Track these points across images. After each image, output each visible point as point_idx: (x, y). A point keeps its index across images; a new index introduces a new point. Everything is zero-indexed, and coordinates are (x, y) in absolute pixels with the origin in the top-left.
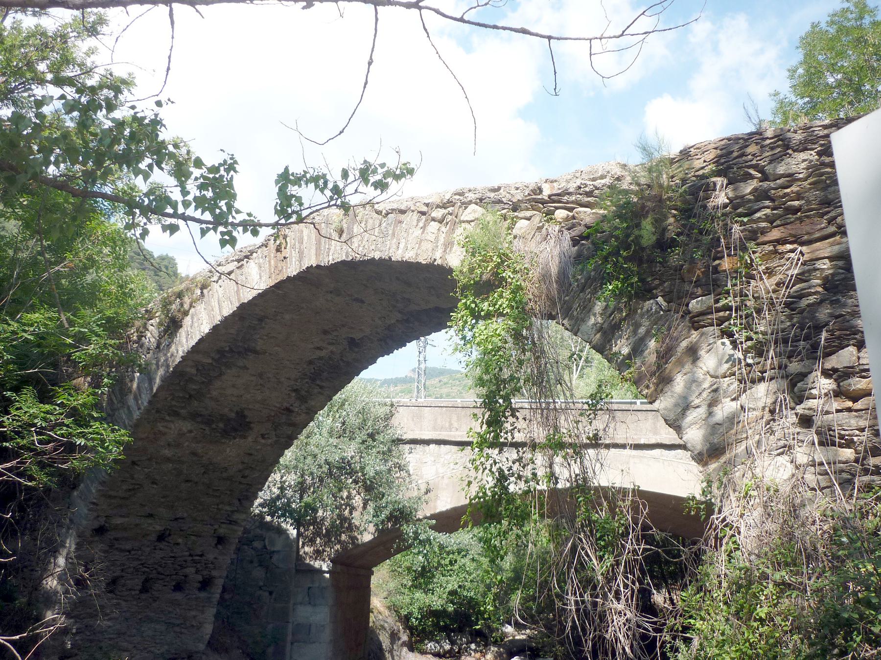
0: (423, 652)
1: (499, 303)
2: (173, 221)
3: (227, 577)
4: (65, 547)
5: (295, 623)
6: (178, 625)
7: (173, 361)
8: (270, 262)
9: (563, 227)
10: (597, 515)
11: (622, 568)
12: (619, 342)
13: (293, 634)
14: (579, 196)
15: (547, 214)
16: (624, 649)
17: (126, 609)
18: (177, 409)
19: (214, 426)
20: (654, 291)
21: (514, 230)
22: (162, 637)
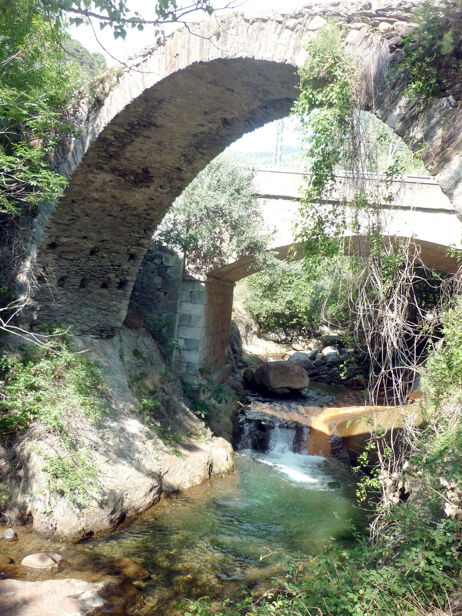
0: (267, 339)
1: (330, 95)
2: (79, 15)
3: (137, 281)
4: (30, 255)
6: (104, 310)
7: (98, 130)
8: (166, 58)
9: (384, 37)
10: (384, 253)
11: (397, 289)
12: (415, 129)
14: (399, 11)
15: (373, 26)
16: (392, 343)
18: (101, 165)
19: (127, 178)
20: (447, 91)
21: (347, 38)
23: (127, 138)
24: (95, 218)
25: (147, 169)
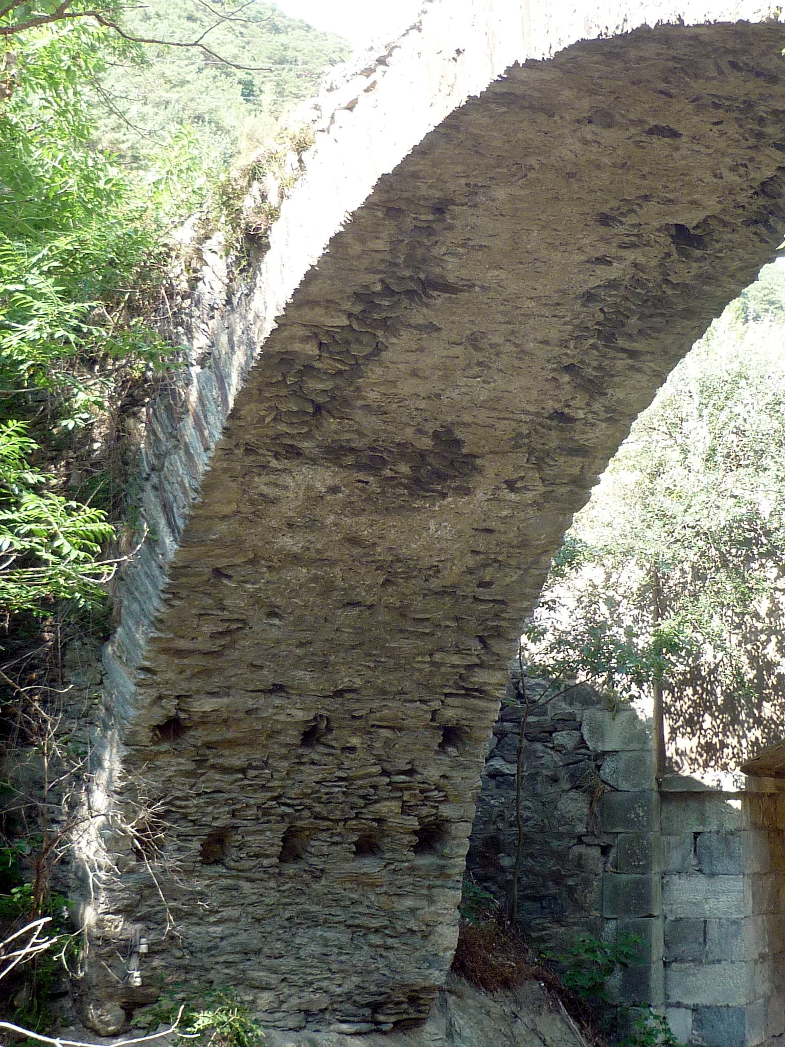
5: (671, 918)
6: (377, 931)
13: (667, 944)
17: (254, 898)
19: (387, 473)
22: (343, 958)
23: (358, 341)
24: (301, 619)
25: (449, 431)
